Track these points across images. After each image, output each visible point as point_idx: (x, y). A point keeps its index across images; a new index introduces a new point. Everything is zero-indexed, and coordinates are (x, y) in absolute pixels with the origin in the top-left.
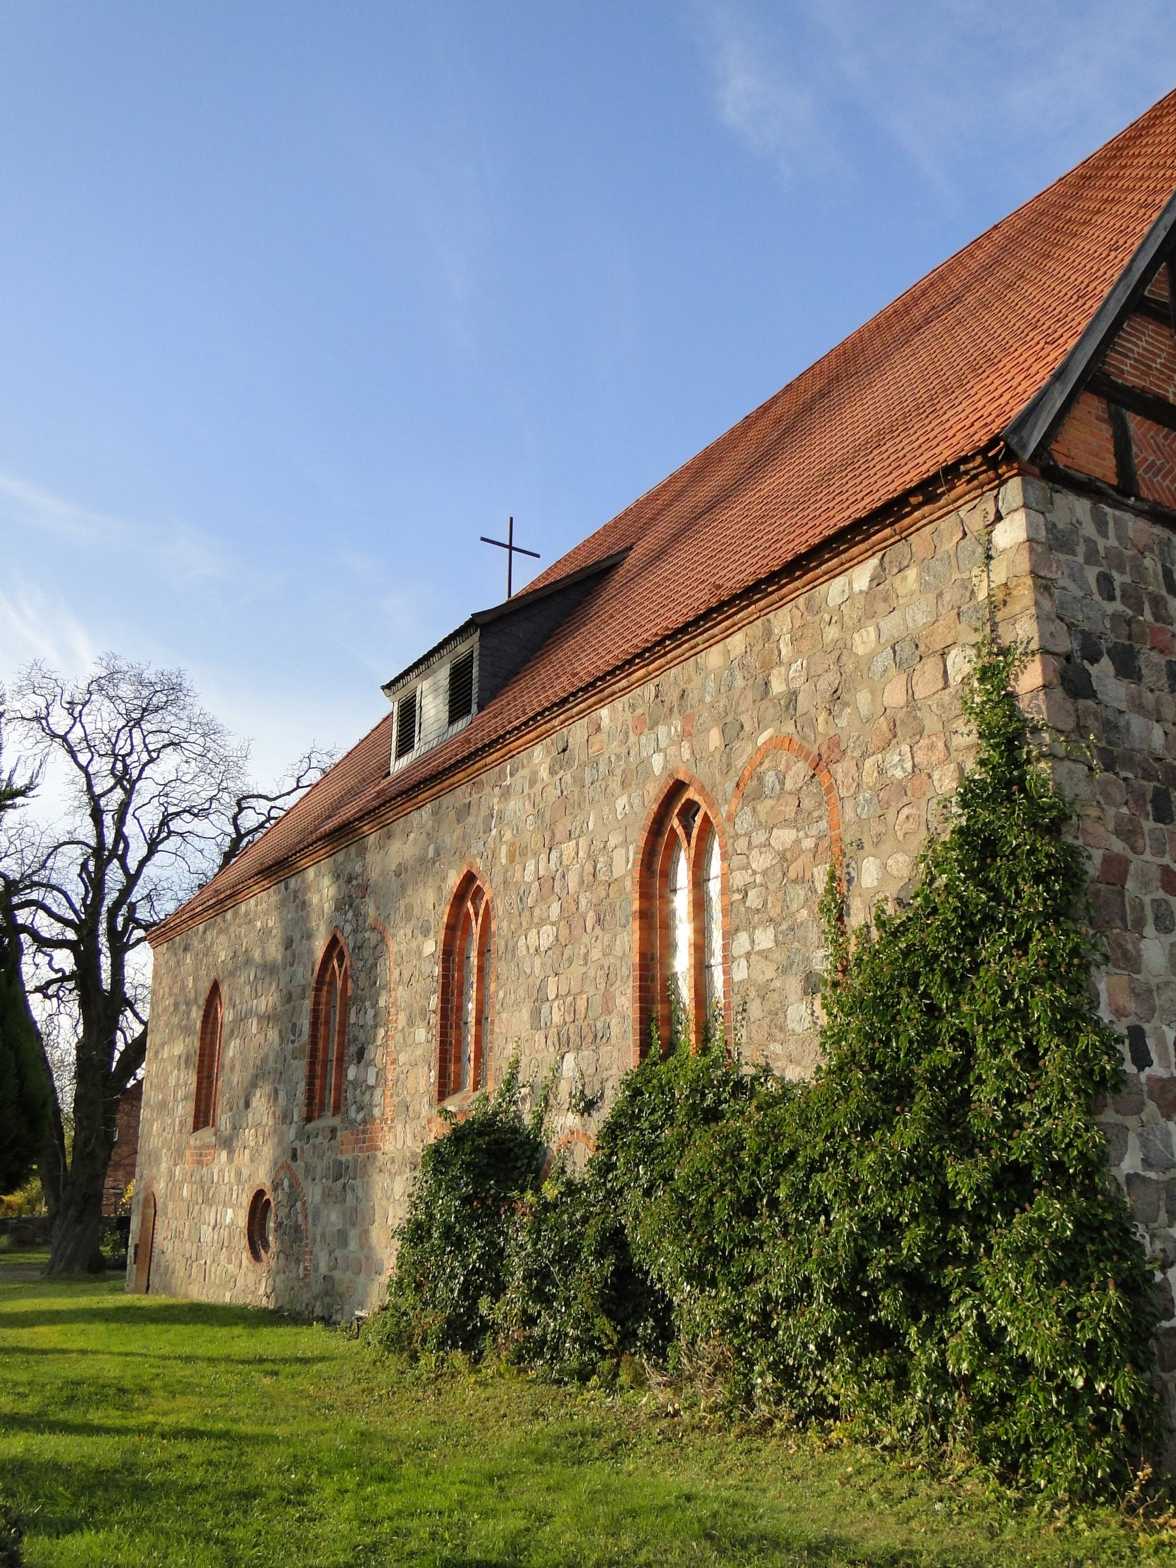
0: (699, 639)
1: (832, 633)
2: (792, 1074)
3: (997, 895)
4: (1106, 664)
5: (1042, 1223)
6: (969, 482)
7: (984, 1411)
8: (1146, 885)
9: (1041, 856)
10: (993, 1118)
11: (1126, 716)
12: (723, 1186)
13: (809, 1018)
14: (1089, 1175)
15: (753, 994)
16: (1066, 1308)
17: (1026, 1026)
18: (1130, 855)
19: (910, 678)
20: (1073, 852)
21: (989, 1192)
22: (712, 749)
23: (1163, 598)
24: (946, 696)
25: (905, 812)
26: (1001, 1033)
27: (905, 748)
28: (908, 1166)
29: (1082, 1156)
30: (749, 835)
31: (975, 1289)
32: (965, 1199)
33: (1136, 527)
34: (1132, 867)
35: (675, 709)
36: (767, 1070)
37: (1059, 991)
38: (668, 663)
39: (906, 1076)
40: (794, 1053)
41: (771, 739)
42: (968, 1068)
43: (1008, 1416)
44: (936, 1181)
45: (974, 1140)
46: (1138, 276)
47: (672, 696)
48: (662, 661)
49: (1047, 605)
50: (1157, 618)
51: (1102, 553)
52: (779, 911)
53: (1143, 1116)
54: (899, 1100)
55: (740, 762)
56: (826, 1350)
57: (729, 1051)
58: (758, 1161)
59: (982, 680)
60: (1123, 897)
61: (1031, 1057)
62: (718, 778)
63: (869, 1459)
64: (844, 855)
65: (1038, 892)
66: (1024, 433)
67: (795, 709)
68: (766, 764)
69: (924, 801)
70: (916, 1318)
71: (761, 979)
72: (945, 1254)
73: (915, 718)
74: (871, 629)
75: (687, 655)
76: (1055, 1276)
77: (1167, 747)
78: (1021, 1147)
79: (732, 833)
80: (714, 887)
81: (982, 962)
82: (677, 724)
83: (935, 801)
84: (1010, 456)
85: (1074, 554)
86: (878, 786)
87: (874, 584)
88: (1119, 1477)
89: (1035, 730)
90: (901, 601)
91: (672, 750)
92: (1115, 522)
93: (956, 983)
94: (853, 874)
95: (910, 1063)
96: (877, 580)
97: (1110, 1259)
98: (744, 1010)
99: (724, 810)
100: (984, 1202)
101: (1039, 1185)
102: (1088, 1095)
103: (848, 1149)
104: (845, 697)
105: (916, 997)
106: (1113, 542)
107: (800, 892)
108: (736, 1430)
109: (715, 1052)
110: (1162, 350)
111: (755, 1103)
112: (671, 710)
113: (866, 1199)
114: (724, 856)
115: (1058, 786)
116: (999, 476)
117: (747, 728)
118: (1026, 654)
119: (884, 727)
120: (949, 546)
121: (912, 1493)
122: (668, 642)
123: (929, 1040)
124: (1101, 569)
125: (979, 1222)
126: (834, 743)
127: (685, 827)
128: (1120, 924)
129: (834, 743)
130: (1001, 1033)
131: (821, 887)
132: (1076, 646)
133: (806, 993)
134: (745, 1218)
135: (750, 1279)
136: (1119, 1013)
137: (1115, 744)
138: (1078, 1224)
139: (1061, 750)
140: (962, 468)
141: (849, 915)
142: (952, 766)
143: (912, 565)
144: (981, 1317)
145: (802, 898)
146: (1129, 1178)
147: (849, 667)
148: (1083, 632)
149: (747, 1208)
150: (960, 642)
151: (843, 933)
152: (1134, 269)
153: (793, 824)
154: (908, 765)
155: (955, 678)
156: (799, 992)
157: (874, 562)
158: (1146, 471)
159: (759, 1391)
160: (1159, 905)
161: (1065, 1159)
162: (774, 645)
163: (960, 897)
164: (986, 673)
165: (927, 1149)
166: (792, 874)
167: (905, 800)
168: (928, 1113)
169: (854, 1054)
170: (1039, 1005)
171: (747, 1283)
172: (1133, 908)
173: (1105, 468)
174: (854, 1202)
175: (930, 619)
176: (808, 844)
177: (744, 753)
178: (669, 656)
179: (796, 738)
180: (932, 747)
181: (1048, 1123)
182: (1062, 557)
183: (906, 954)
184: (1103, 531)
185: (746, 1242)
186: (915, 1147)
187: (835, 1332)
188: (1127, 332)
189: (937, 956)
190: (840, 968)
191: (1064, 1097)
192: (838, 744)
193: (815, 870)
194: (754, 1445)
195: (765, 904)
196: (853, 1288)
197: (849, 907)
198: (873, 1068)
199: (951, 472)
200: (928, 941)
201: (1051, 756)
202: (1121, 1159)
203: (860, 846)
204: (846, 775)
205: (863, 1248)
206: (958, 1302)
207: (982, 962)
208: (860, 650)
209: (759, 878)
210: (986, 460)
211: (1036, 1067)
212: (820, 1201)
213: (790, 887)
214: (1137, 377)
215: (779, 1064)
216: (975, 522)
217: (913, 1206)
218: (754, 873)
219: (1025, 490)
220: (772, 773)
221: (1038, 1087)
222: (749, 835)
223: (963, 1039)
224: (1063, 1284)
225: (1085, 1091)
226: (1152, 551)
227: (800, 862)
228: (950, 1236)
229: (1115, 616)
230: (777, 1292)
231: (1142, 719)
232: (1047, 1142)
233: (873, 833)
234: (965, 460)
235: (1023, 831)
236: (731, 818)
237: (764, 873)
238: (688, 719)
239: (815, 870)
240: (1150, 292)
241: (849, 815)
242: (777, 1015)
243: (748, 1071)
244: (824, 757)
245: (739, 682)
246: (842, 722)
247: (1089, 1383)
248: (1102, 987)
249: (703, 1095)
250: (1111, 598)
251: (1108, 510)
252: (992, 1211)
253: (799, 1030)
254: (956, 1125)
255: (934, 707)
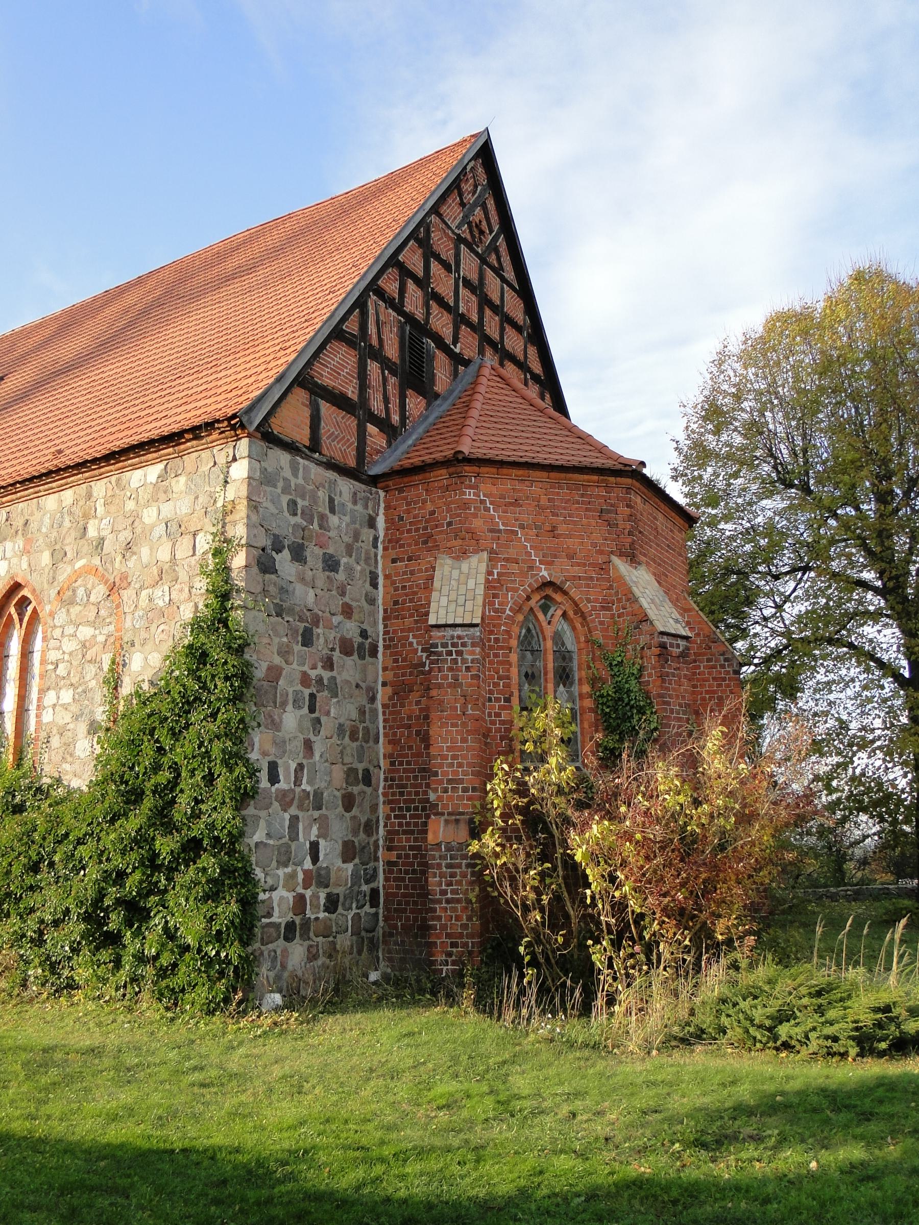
0: (41, 488)
1: (130, 505)
2: (75, 783)
3: (204, 687)
4: (286, 553)
5: (204, 870)
6: (220, 433)
7: (163, 973)
8: (291, 682)
9: (229, 666)
10: (186, 813)
11: (294, 585)
12: (20, 854)
13: (90, 749)
14: (233, 844)
15: (55, 731)
16: (209, 914)
17: (210, 761)
18: (284, 665)
19: (174, 545)
20: (248, 664)
21: (178, 854)
22: (43, 565)
23: (326, 515)
24: (193, 560)
25: (162, 627)
26: (195, 765)
27: (166, 588)
28: (135, 840)
29: (230, 833)
30: (62, 627)
31: (165, 908)
32: (165, 858)
33: (317, 472)
34: (284, 673)
35: (20, 532)
36: (59, 781)
37: (229, 744)
38: (17, 499)
39: (141, 789)
40: (78, 771)
41: (84, 566)
42: (177, 784)
43: (174, 975)
44: (150, 848)
45: (174, 825)
46: (338, 319)
47: (18, 523)
48: (14, 497)
49: (254, 518)
50: (321, 527)
51: (293, 487)
52: (77, 679)
53: (270, 811)
54: (135, 802)
55: (62, 578)
56: (75, 950)
57: (35, 768)
58: (44, 839)
59: (214, 555)
60: (276, 688)
61: (210, 779)
62: (46, 586)
63: (94, 1007)
64: (123, 649)
65: (226, 687)
66: (252, 414)
67: (102, 550)
68: (79, 582)
69: (173, 623)
70: (131, 926)
71: (61, 722)
72: (151, 889)
73: (174, 570)
74: (155, 509)
75: (32, 497)
76: (206, 898)
77: (316, 602)
78: (198, 829)
79: (52, 625)
80: (36, 658)
81: (191, 724)
82: (20, 542)
83: (179, 624)
84: (243, 427)
85: (275, 486)
86: (148, 609)
87: (160, 480)
88: (227, 1000)
89: (238, 591)
90: (174, 496)
91: (15, 561)
92: (304, 468)
93: (175, 735)
94: (127, 661)
95: (144, 780)
96: (162, 478)
97: (236, 887)
98: (48, 742)
99: (48, 608)
100: (176, 859)
101: (205, 850)
102: (237, 800)
103: (101, 831)
104: (134, 549)
105: (152, 742)
106: (300, 481)
107: (91, 670)
108: (14, 1002)
109: (27, 764)
110: (347, 363)
111: (48, 802)
112: (17, 532)
113: (108, 860)
114: (45, 639)
115: (246, 625)
116: (237, 435)
117: (70, 555)
118: (238, 545)
119: (155, 572)
120: (205, 468)
121: (114, 1021)
122: (18, 485)
123: (157, 768)
124: (291, 497)
125: (171, 871)
126: (124, 577)
127: (19, 614)
128: (272, 704)
129: (124, 577)
130: (195, 765)
131: (106, 667)
132: (269, 543)
133: (89, 733)
134: (31, 874)
135: (32, 910)
136: (265, 754)
137: (285, 601)
138: (221, 868)
139: (250, 605)
140: (216, 425)
141: (121, 687)
142: (192, 604)
143: (183, 474)
144: (167, 922)
145: (93, 673)
146: (257, 844)
147: (138, 530)
148: (274, 535)
149: (35, 868)
150: (204, 530)
151: (117, 698)
152: (336, 314)
153: (92, 624)
154: (167, 599)
155: (200, 551)
156: (85, 732)
157: (161, 466)
158: (328, 438)
159: (32, 979)
160: (297, 694)
161: (221, 835)
162: (93, 504)
163: (184, 686)
164: (217, 553)
165: (146, 831)
166: (88, 657)
167: (163, 620)
168: (151, 810)
169: (112, 774)
170: (216, 749)
171: (30, 913)
172: (281, 695)
173: (302, 436)
174: (101, 862)
175: (190, 511)
176: (101, 639)
177: (65, 572)
178: (19, 494)
179: (100, 568)
180: (181, 590)
181: (214, 815)
182: (269, 489)
183: (149, 716)
184: (295, 475)
185: (31, 888)
186: (140, 829)
187: (82, 938)
188: (330, 352)
189: (166, 719)
190: (112, 719)
191: (224, 803)
192: (126, 578)
193: (104, 656)
194: (24, 1009)
195: (69, 674)
196: (95, 911)
197: (122, 681)
198: (122, 783)
199: (209, 426)
200: (163, 709)
201: (244, 607)
202: (254, 834)
203: (133, 645)
204: (129, 598)
205: (103, 888)
206: (155, 915)
207: (191, 724)
208: (147, 520)
209: (67, 657)
210: (230, 425)
211: (212, 785)
212: (80, 862)
213: (86, 665)
214: (330, 379)
215: (67, 777)
216: (222, 459)
217: (134, 863)
218: (64, 653)
219: (250, 446)
220: (82, 589)
221: (211, 796)
222: (62, 627)
223: (175, 769)
224: (210, 902)
225: (235, 798)
226: (324, 487)
227: (94, 649)
228: (154, 879)
229: (296, 526)
230: (48, 918)
231: (303, 587)
232: (212, 826)
233: (142, 637)
234: (218, 421)
235: (222, 651)
236: (52, 614)
237: (70, 654)
238: (28, 541)
239: (104, 656)
240: (347, 327)
241: (128, 624)
242: (68, 748)
243: (46, 781)
244: (117, 584)
245: (67, 524)
246: (130, 564)
247: (218, 953)
248: (256, 740)
249: (14, 796)
250: (295, 514)
251: (301, 460)
252: (179, 864)
253: (82, 756)
254: (166, 816)
255: (185, 566)
